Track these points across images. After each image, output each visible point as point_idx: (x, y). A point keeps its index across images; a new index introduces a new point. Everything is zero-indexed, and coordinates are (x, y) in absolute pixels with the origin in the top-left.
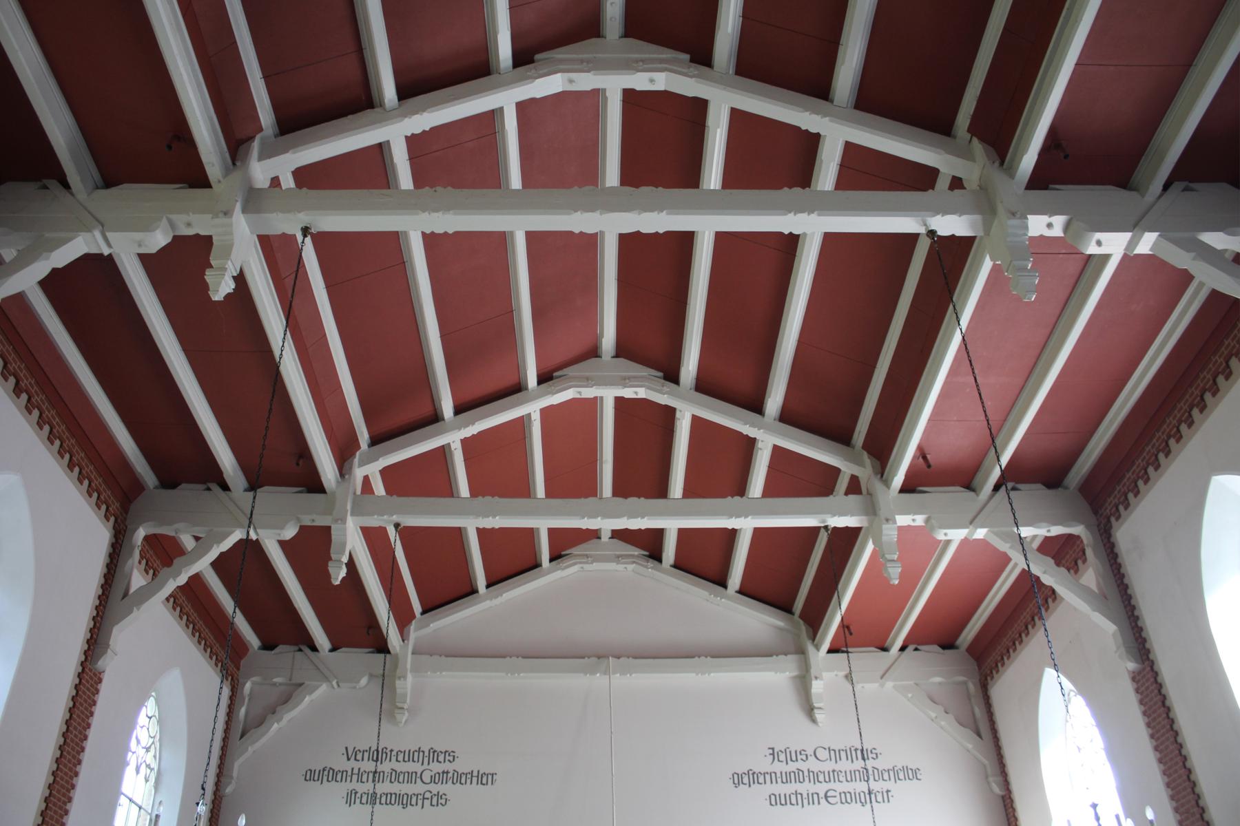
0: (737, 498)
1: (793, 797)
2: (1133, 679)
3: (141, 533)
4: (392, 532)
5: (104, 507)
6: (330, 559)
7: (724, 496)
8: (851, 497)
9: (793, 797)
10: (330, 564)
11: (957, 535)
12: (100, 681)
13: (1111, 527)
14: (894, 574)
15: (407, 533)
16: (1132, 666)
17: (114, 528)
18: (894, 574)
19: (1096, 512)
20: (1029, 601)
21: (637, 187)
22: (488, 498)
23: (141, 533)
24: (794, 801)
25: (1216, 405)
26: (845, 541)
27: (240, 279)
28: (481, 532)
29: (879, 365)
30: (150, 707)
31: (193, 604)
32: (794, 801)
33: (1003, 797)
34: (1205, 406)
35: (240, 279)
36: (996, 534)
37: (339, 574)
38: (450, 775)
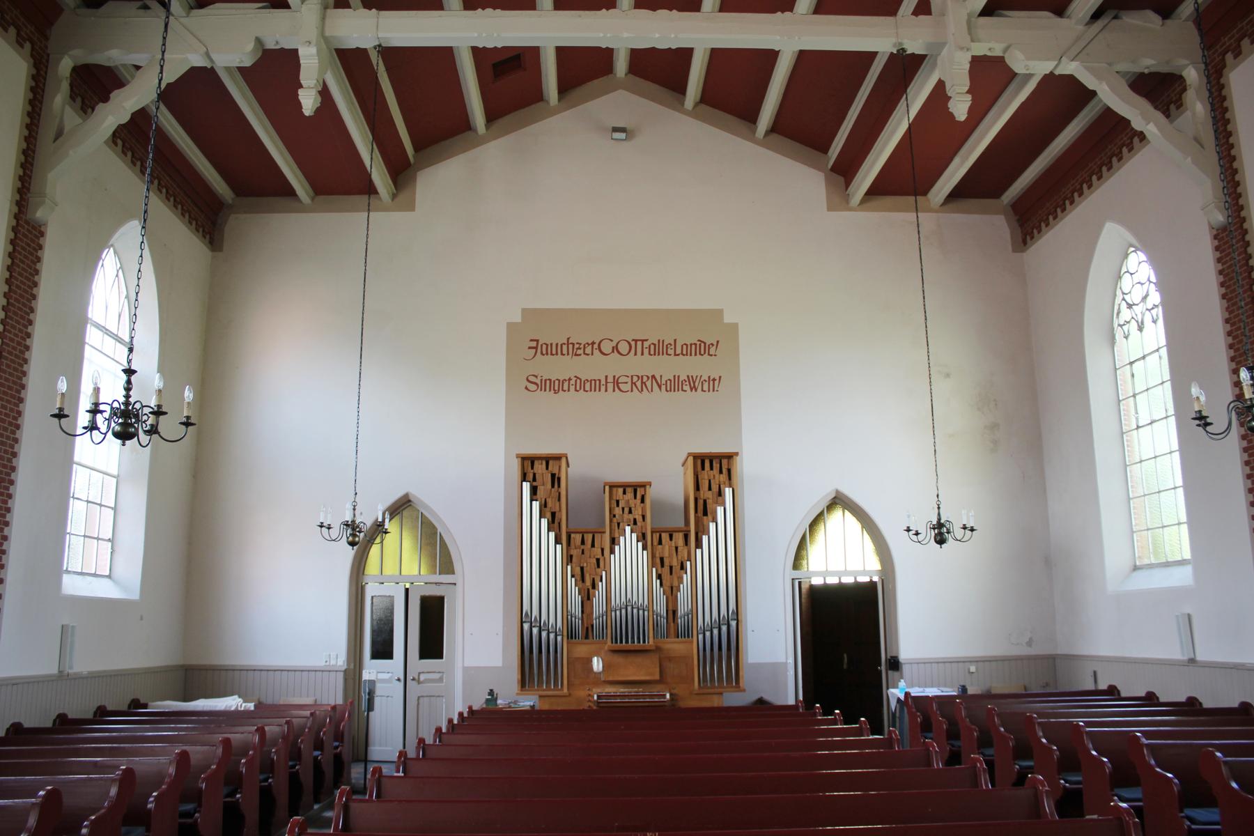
0: (787, 14)
1: (565, 347)
2: (1215, 237)
3: (65, 66)
4: (374, 57)
5: (129, 154)
6: (301, 86)
7: (774, 11)
8: (921, 17)
9: (565, 347)
10: (300, 92)
11: (1042, 68)
12: (42, 234)
13: (1224, 66)
14: (960, 108)
15: (390, 54)
16: (1220, 218)
17: (32, 56)
18: (960, 108)
19: (1021, 226)
20: (1110, 141)
21: (654, 10)
22: (489, 10)
23: (65, 66)
24: (565, 351)
25: (1236, 66)
26: (905, 67)
27: (325, 93)
28: (479, 54)
29: (863, 88)
30: (109, 263)
31: (135, 138)
32: (565, 351)
33: (1223, 229)
34: (1240, 53)
35: (325, 93)
36: (1087, 68)
37: (308, 102)
38: (573, 382)
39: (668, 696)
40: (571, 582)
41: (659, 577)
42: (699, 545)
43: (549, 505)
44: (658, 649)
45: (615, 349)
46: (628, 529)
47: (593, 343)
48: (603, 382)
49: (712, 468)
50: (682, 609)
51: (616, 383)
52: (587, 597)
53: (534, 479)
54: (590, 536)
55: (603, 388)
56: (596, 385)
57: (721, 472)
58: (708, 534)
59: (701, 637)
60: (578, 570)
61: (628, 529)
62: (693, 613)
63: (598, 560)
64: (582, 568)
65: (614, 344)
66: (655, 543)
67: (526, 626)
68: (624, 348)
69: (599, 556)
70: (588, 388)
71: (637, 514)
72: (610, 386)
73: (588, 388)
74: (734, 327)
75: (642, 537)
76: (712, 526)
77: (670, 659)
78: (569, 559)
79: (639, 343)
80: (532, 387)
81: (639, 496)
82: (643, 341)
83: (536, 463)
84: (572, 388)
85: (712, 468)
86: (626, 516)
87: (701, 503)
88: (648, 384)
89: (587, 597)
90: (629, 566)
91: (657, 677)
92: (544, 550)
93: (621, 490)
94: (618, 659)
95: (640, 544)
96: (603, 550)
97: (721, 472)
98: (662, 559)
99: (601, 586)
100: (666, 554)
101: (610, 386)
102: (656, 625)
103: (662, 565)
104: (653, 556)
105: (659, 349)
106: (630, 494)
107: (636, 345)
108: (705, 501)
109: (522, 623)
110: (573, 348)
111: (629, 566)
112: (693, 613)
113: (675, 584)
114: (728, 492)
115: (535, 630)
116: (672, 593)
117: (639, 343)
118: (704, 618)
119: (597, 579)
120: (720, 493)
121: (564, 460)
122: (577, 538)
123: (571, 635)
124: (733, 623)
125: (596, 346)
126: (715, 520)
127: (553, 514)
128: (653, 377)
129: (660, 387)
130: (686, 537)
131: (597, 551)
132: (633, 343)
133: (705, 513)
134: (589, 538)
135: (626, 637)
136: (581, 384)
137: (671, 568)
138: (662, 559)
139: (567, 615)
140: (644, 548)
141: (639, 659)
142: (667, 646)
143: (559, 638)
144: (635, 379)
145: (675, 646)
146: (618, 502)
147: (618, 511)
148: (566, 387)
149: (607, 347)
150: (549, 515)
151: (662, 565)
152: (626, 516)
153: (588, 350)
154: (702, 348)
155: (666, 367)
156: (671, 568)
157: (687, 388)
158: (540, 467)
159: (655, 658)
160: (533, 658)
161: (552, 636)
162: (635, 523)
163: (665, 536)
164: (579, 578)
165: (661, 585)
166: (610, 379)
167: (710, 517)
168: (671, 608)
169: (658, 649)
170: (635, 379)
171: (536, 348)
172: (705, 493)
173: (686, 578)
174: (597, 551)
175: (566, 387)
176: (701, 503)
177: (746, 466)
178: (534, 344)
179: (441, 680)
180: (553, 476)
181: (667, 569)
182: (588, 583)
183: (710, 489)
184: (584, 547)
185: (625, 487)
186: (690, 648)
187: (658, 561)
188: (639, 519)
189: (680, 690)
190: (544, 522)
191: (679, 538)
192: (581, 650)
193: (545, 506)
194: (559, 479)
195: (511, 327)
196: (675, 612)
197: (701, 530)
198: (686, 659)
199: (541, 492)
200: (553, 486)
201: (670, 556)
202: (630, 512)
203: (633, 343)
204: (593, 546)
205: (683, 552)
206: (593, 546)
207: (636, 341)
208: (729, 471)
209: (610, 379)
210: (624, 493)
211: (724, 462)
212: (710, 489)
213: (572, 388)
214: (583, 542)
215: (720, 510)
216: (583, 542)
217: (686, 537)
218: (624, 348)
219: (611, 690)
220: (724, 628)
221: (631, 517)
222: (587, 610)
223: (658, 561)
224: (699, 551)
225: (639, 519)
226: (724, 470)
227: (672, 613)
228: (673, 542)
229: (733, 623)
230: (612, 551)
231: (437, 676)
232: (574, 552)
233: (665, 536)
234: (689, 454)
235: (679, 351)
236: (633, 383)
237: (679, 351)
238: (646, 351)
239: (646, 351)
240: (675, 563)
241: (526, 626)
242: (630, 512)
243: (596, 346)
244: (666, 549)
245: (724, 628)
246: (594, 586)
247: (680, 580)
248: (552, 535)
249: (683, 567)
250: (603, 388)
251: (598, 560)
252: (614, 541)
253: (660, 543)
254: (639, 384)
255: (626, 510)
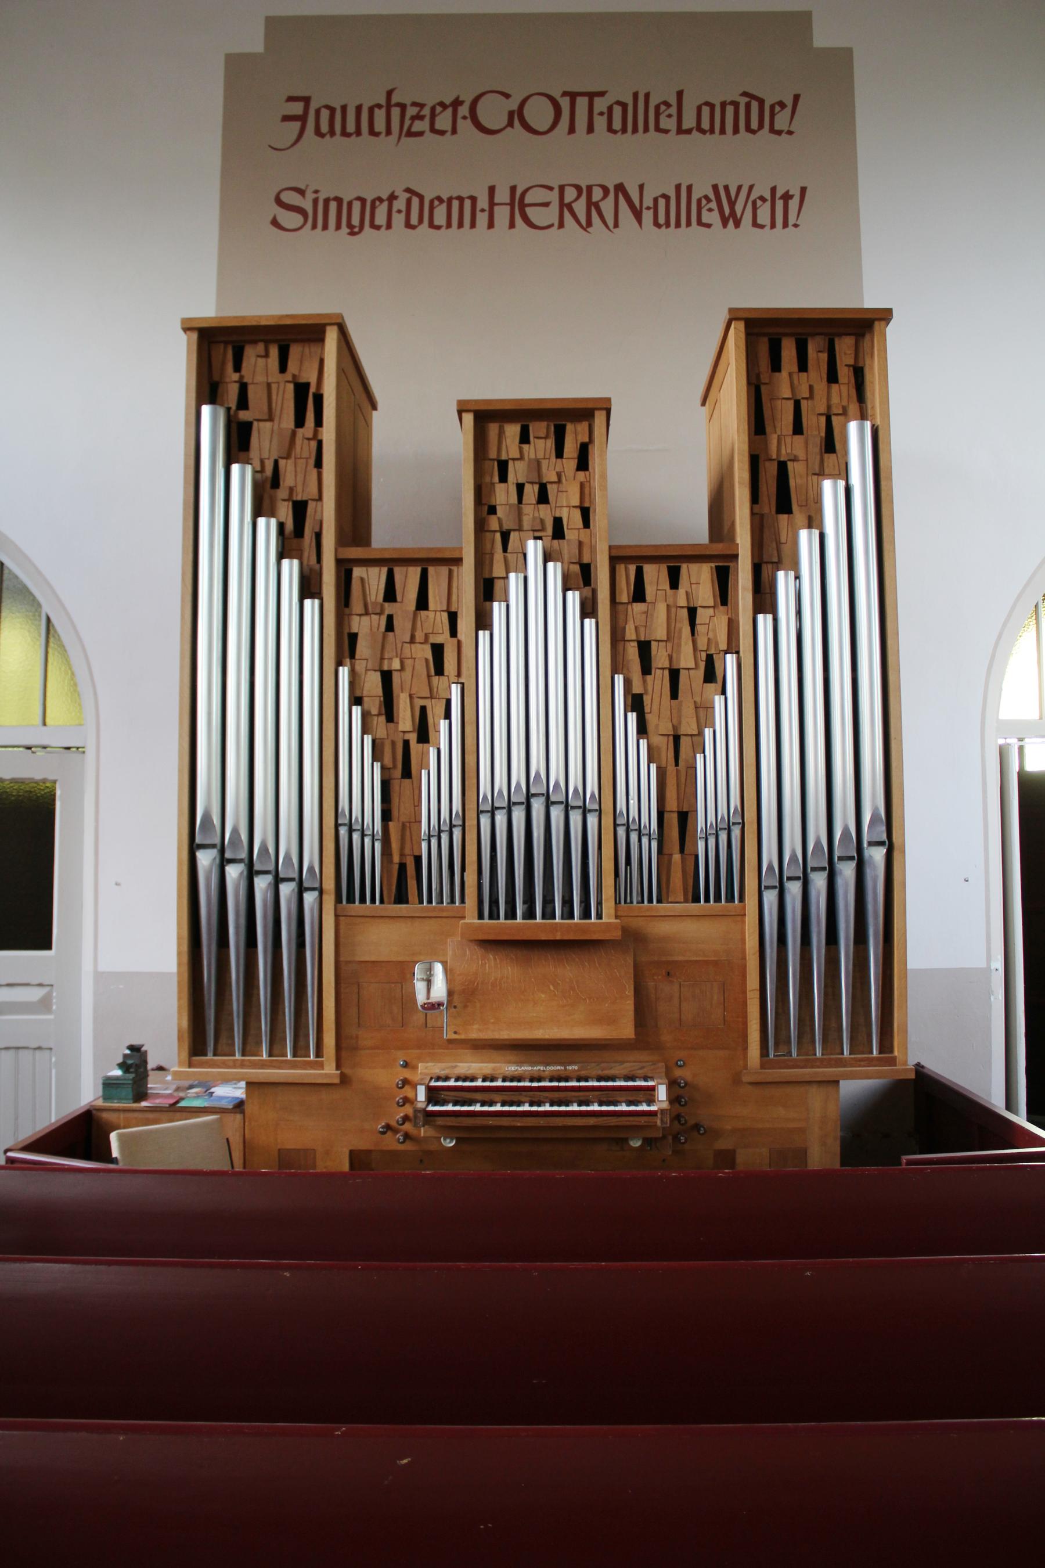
1: (380, 115)
9: (380, 115)
24: (380, 125)
32: (380, 125)
38: (400, 204)
39: (662, 1093)
40: (350, 717)
41: (636, 703)
42: (764, 599)
43: (288, 479)
44: (632, 939)
45: (517, 116)
46: (534, 549)
47: (457, 103)
48: (483, 203)
49: (803, 367)
50: (708, 811)
51: (519, 204)
52: (400, 769)
53: (243, 402)
54: (414, 574)
55: (482, 219)
56: (462, 211)
57: (832, 377)
58: (795, 566)
59: (770, 898)
60: (373, 684)
61: (534, 549)
62: (744, 820)
63: (438, 651)
64: (387, 677)
65: (513, 105)
66: (624, 595)
67: (205, 859)
68: (539, 113)
69: (443, 637)
70: (440, 218)
71: (565, 503)
72: (502, 214)
73: (440, 218)
74: (841, 61)
75: (580, 577)
76: (806, 540)
77: (670, 970)
78: (347, 646)
79: (582, 103)
80: (296, 220)
81: (571, 448)
82: (591, 96)
83: (251, 354)
84: (398, 220)
85: (803, 367)
86: (531, 510)
87: (770, 471)
88: (607, 207)
89: (400, 769)
90: (535, 688)
91: (627, 1030)
92: (275, 624)
93: (513, 431)
94: (501, 969)
95: (574, 598)
96: (453, 618)
97: (832, 377)
98: (644, 648)
99: (446, 733)
100: (660, 632)
101: (502, 214)
102: (624, 860)
103: (646, 669)
104: (617, 637)
105: (636, 116)
106: (541, 447)
107: (573, 109)
108: (782, 467)
109: (193, 848)
110: (403, 118)
111: (535, 688)
112: (744, 820)
113: (689, 727)
114: (855, 436)
115: (233, 872)
116: (675, 757)
117: (582, 103)
118: (785, 834)
119: (435, 710)
120: (831, 443)
121: (332, 337)
122: (372, 580)
123: (349, 890)
124: (877, 856)
125: (464, 110)
126: (814, 521)
127: (300, 509)
128: (620, 188)
129: (638, 215)
130: (723, 579)
131: (435, 619)
132: (565, 103)
133: (784, 506)
134: (408, 581)
135: (531, 900)
136: (422, 210)
137: (674, 675)
138: (644, 648)
139: (338, 823)
140: (588, 610)
141: (568, 971)
142: (664, 928)
143: (309, 898)
144: (570, 194)
145: (685, 928)
146: (503, 468)
147: (503, 495)
148: (381, 218)
149: (492, 112)
150: (285, 512)
151: (646, 669)
152: (531, 510)
153: (444, 121)
154: (753, 115)
155: (653, 163)
156: (674, 675)
157: (712, 217)
158: (259, 366)
159: (622, 968)
160: (232, 969)
161: (287, 890)
162: (558, 531)
163: (655, 576)
164: (374, 704)
165: (642, 730)
166: (502, 195)
167: (799, 515)
168: (672, 804)
169: (632, 939)
170: (570, 194)
171: (303, 119)
172: (782, 442)
173: (724, 708)
174: (435, 619)
175: (381, 218)
176: (770, 471)
177: (904, 363)
178: (297, 108)
179: (44, 1005)
180: (301, 390)
181: (659, 681)
182: (405, 721)
183: (798, 428)
184: (387, 607)
185: (525, 416)
186: (740, 933)
187: (632, 652)
188: (572, 519)
189: (703, 1070)
190: (267, 528)
191: (700, 580)
192: (382, 937)
193: (276, 481)
194: (319, 399)
195: (237, 66)
196: (685, 818)
197: (771, 557)
198: (724, 969)
199: (265, 441)
200: (300, 422)
201: (671, 636)
202: (543, 498)
203: (565, 103)
204: (422, 603)
205: (714, 625)
206: (422, 603)
207: (573, 96)
208: (859, 374)
209: (502, 195)
210: (525, 439)
211: (845, 347)
212: (798, 428)
213: (398, 220)
214: (390, 594)
215: (830, 491)
216: (390, 594)
217: (723, 579)
218: (539, 113)
219: (476, 1067)
220: (847, 872)
221: (546, 513)
222: (401, 810)
223: (630, 654)
224: (764, 621)
225: (572, 519)
226: (844, 374)
227: (677, 820)
228: (675, 611)
229: (877, 856)
230: (483, 622)
231: (34, 995)
232: (362, 625)
233: (655, 576)
234: (735, 315)
235: (689, 122)
236: (565, 206)
237: (689, 122)
238: (600, 123)
239: (600, 123)
240: (686, 659)
241: (205, 859)
242: (543, 498)
243: (464, 110)
244: (655, 617)
245: (847, 872)
246: (424, 734)
247: (704, 713)
248: (291, 568)
249: (711, 674)
250: (482, 219)
251: (438, 651)
252: (488, 590)
253: (639, 595)
254: (580, 207)
255: (531, 493)
